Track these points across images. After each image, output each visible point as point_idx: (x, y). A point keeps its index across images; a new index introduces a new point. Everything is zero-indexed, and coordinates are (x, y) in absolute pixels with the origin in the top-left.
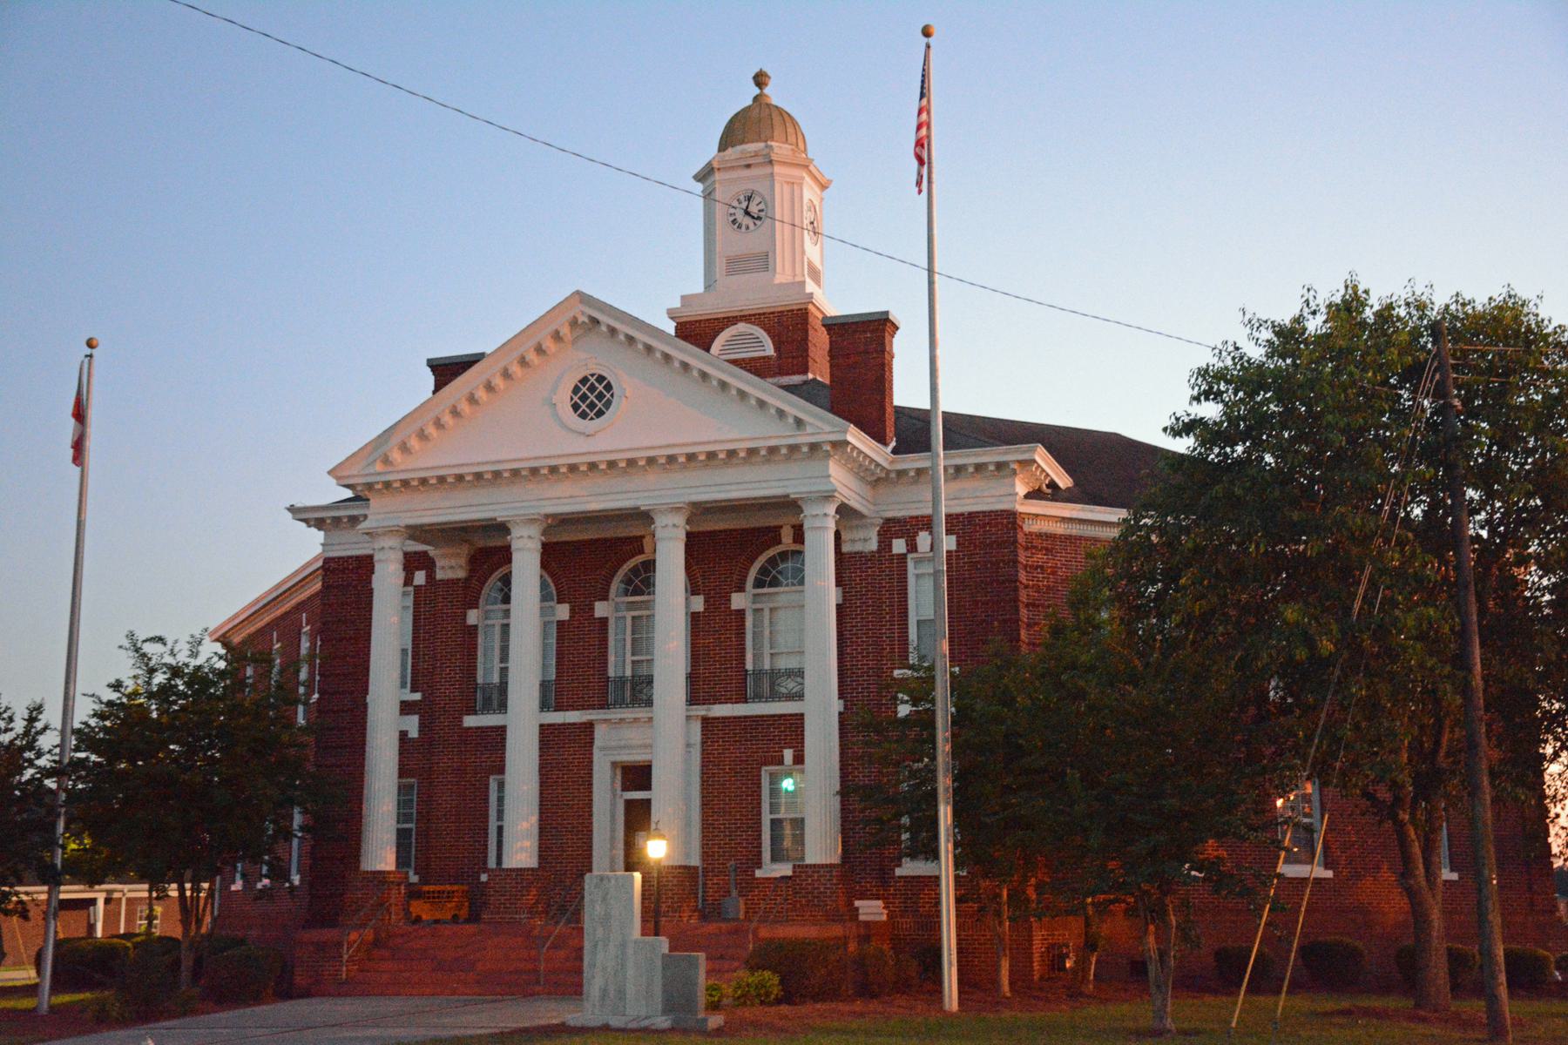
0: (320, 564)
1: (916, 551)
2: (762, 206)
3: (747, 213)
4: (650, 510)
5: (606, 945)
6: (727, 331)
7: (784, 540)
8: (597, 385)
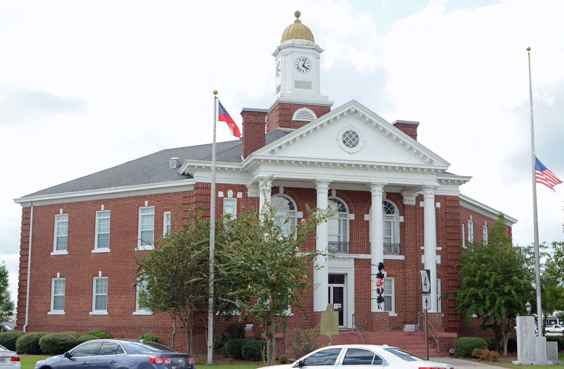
2: (309, 64)
3: (303, 66)
5: (526, 339)
6: (299, 109)
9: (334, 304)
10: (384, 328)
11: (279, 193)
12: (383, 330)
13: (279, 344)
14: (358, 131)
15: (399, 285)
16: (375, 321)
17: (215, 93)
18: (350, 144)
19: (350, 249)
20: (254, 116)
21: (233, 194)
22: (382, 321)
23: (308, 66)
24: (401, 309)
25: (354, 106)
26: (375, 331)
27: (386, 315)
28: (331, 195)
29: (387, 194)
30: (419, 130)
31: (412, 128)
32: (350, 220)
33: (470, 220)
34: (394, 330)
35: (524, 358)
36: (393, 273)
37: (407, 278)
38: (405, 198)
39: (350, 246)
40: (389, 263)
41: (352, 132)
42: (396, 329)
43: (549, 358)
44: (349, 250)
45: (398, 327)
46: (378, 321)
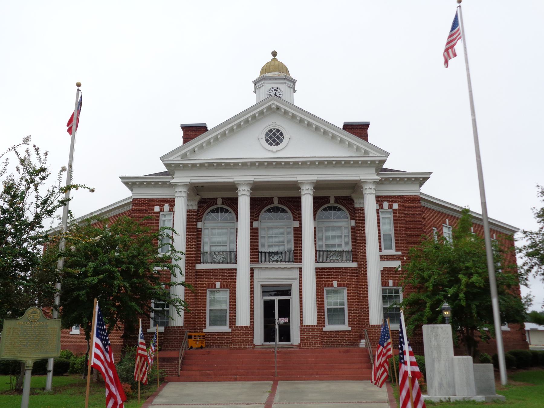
0: (131, 200)
1: (383, 209)
2: (280, 93)
4: (359, 181)
5: (439, 361)
7: (274, 203)
8: (276, 133)
9: (280, 318)
10: (314, 344)
11: (217, 204)
12: (312, 346)
13: (173, 364)
14: (281, 127)
15: (352, 295)
16: (304, 336)
17: (79, 85)
18: (273, 143)
19: (294, 258)
20: (192, 131)
21: (170, 208)
22: (312, 335)
23: (280, 95)
24: (355, 322)
25: (274, 101)
26: (303, 348)
27: (317, 328)
28: (273, 203)
29: (335, 198)
30: (369, 131)
31: (362, 129)
32: (294, 228)
33: (446, 224)
34: (348, 346)
35: (435, 391)
36: (344, 282)
37: (361, 287)
38: (355, 202)
39: (294, 255)
40: (340, 271)
41: (275, 130)
42: (350, 345)
43: (480, 392)
44: (294, 260)
45: (353, 343)
46: (307, 335)
